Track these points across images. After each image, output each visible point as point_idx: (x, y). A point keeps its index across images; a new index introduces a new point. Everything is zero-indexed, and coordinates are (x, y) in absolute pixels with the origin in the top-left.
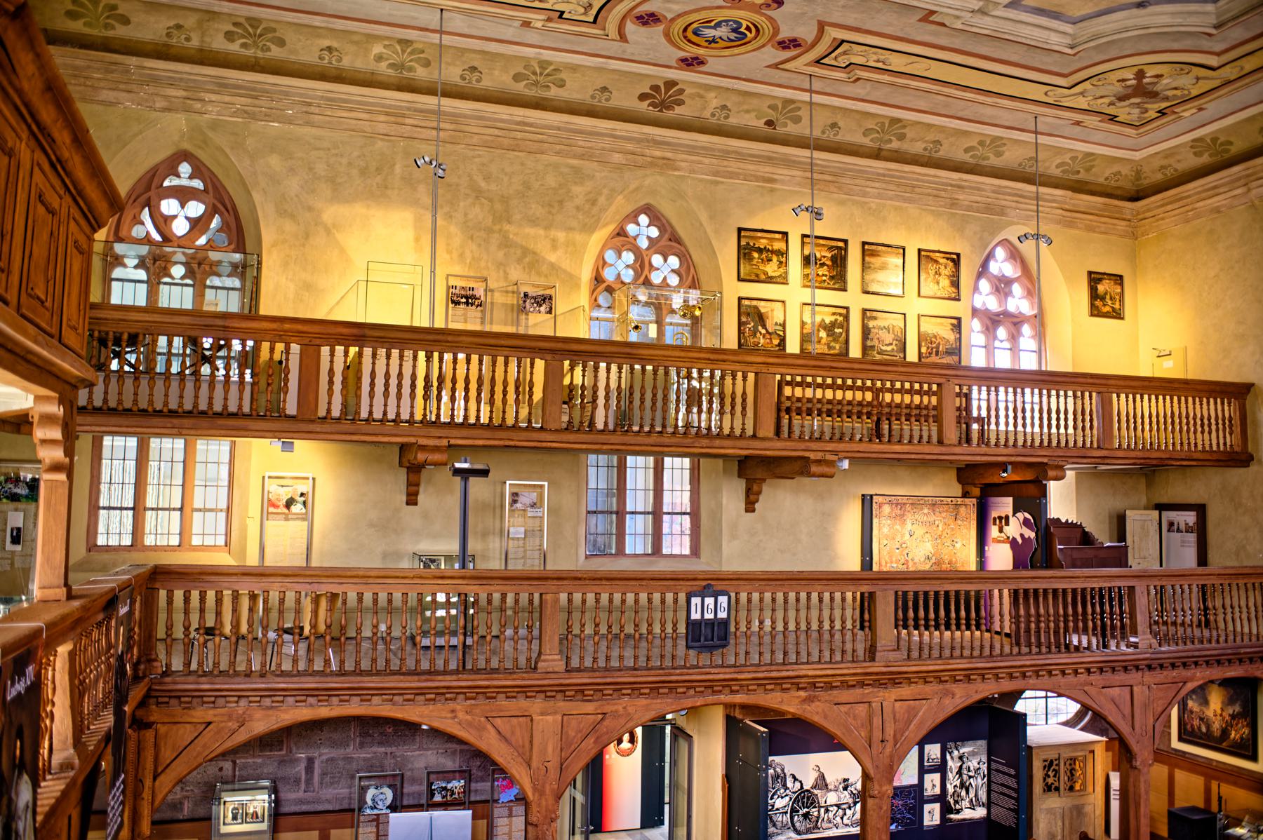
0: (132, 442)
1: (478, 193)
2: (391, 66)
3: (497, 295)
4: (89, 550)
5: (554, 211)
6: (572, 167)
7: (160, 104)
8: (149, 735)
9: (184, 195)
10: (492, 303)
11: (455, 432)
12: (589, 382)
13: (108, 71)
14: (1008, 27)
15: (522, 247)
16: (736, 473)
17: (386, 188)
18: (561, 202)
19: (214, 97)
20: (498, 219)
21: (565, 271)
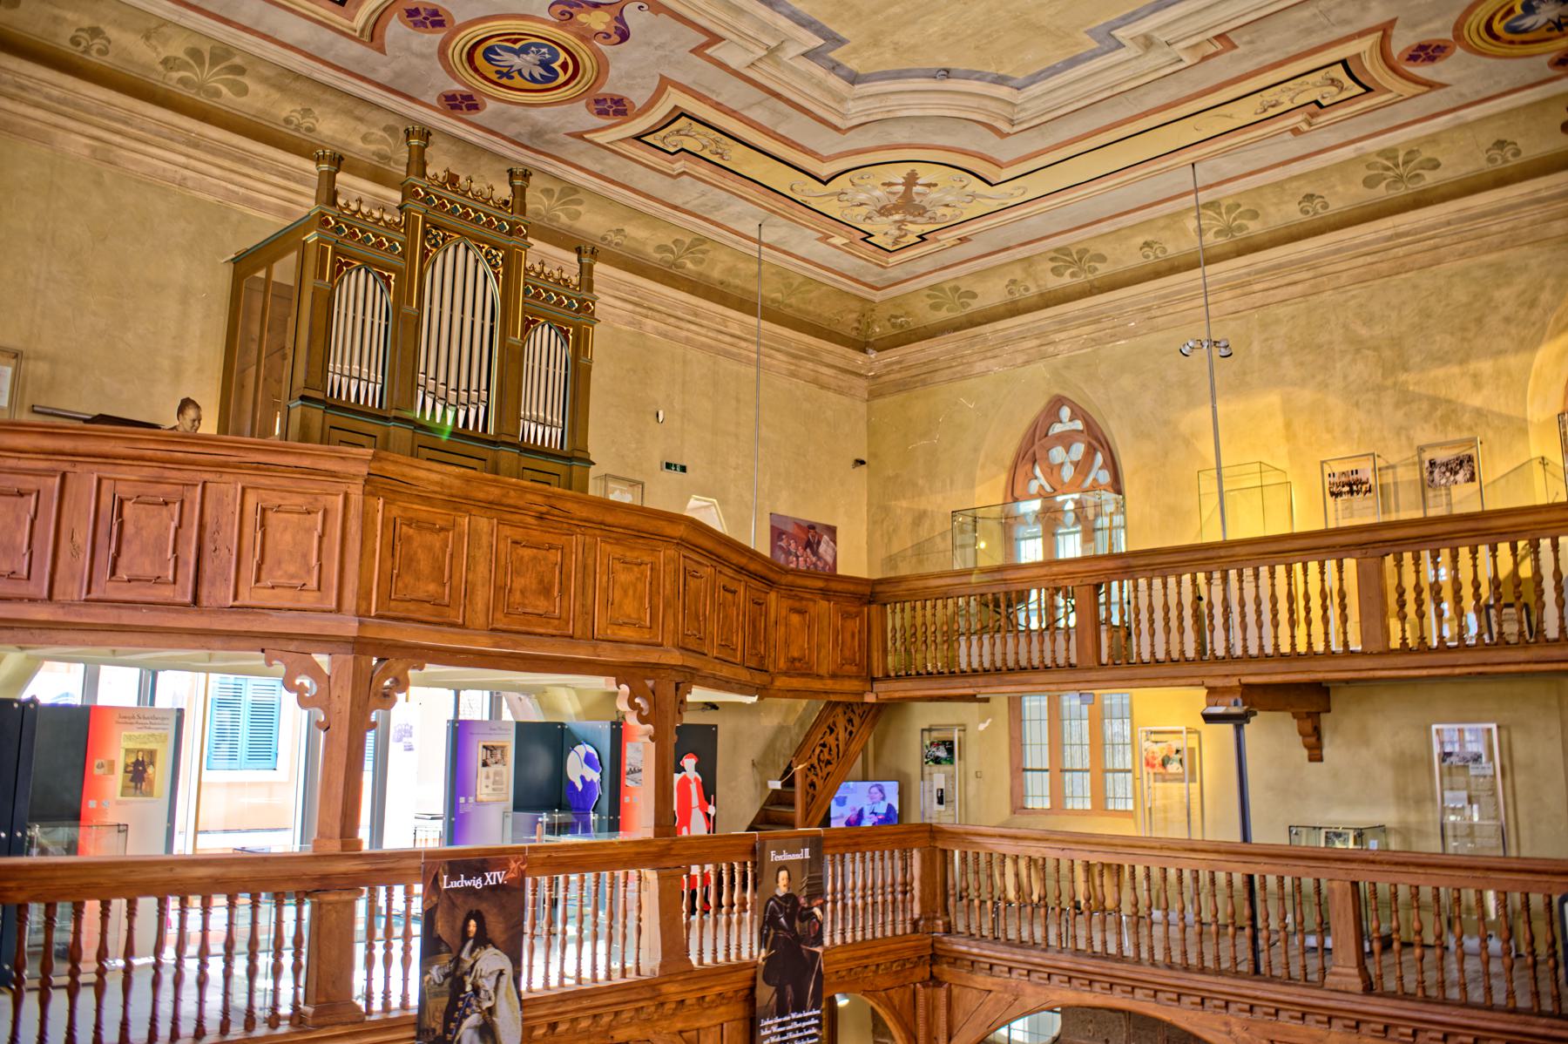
0: (1044, 701)
1: (1358, 345)
2: (1218, 233)
3: (1400, 471)
4: (1014, 812)
5: (1470, 335)
6: (1490, 265)
7: (1020, 359)
8: (942, 993)
9: (1066, 440)
10: (1395, 484)
11: (1253, 667)
12: (1526, 571)
13: (972, 345)
15: (1429, 398)
16: (42, 737)
17: (1245, 373)
18: (1479, 321)
19: (1062, 336)
20: (1389, 370)
21: (1500, 415)
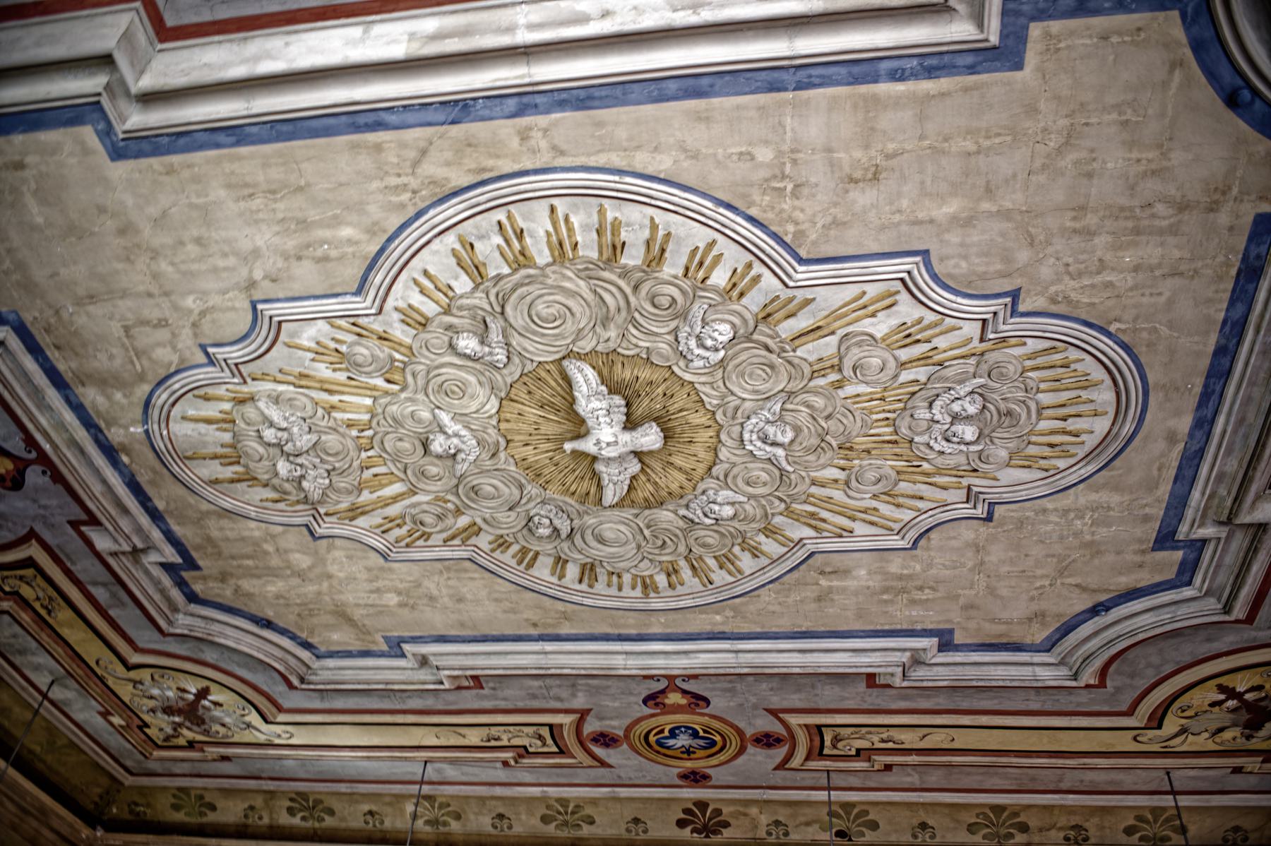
2: (428, 822)
14: (971, 672)
